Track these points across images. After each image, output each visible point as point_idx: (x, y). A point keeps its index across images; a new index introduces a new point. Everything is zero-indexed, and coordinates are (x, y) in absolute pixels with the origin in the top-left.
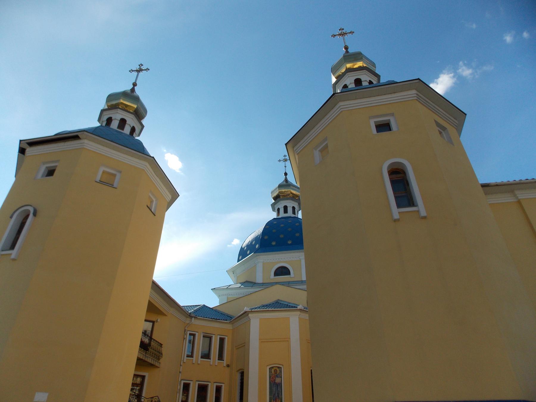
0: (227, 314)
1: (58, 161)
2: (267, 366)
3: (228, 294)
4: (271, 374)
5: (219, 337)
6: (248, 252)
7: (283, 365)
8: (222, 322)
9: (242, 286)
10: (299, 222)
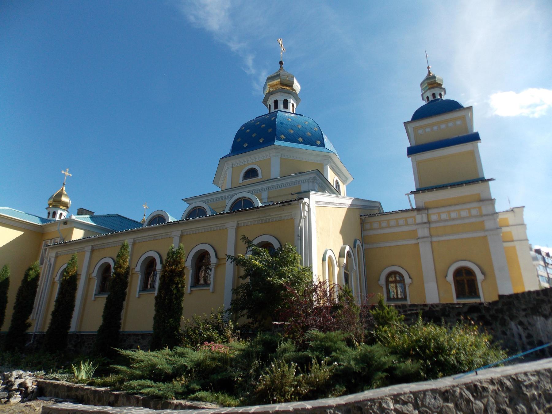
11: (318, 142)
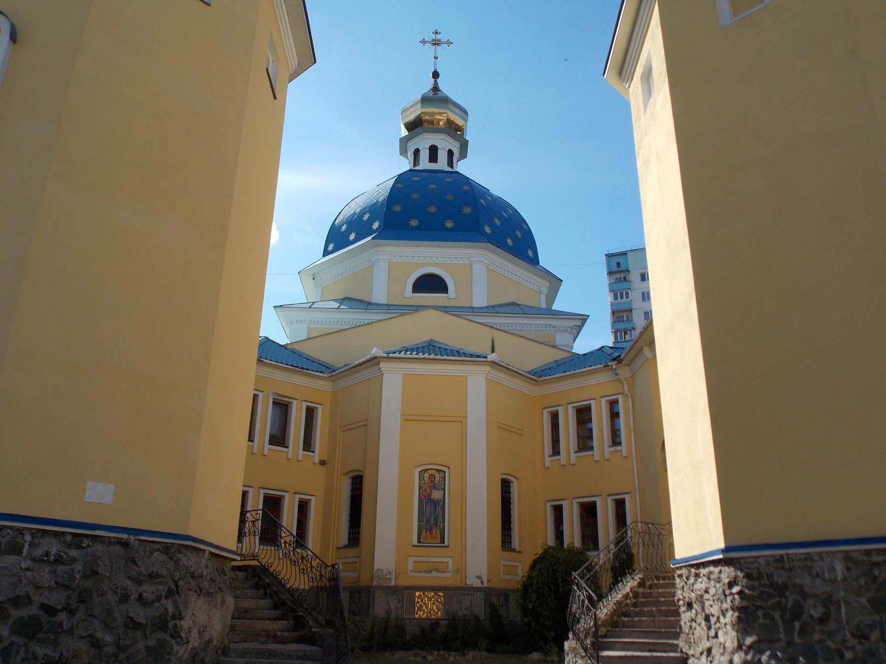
3: (311, 321)
5: (305, 405)
7: (449, 468)
9: (342, 307)
11: (530, 253)
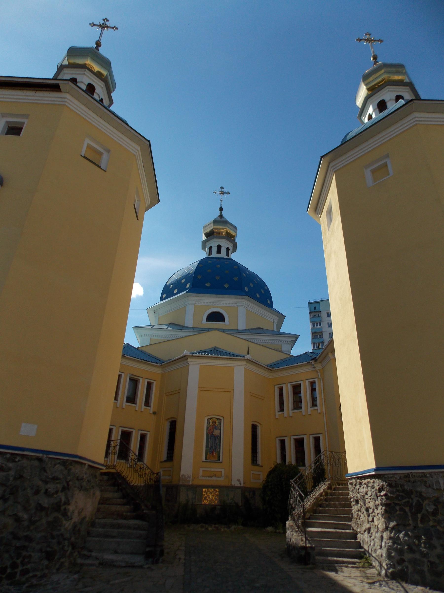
0: (155, 357)
1: (26, 116)
2: (205, 416)
3: (152, 335)
4: (209, 425)
5: (146, 380)
6: (176, 291)
8: (152, 365)
9: (169, 328)
10: (238, 266)
